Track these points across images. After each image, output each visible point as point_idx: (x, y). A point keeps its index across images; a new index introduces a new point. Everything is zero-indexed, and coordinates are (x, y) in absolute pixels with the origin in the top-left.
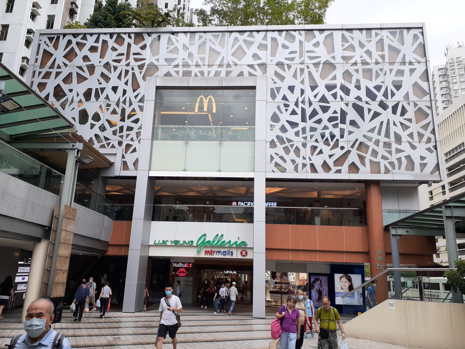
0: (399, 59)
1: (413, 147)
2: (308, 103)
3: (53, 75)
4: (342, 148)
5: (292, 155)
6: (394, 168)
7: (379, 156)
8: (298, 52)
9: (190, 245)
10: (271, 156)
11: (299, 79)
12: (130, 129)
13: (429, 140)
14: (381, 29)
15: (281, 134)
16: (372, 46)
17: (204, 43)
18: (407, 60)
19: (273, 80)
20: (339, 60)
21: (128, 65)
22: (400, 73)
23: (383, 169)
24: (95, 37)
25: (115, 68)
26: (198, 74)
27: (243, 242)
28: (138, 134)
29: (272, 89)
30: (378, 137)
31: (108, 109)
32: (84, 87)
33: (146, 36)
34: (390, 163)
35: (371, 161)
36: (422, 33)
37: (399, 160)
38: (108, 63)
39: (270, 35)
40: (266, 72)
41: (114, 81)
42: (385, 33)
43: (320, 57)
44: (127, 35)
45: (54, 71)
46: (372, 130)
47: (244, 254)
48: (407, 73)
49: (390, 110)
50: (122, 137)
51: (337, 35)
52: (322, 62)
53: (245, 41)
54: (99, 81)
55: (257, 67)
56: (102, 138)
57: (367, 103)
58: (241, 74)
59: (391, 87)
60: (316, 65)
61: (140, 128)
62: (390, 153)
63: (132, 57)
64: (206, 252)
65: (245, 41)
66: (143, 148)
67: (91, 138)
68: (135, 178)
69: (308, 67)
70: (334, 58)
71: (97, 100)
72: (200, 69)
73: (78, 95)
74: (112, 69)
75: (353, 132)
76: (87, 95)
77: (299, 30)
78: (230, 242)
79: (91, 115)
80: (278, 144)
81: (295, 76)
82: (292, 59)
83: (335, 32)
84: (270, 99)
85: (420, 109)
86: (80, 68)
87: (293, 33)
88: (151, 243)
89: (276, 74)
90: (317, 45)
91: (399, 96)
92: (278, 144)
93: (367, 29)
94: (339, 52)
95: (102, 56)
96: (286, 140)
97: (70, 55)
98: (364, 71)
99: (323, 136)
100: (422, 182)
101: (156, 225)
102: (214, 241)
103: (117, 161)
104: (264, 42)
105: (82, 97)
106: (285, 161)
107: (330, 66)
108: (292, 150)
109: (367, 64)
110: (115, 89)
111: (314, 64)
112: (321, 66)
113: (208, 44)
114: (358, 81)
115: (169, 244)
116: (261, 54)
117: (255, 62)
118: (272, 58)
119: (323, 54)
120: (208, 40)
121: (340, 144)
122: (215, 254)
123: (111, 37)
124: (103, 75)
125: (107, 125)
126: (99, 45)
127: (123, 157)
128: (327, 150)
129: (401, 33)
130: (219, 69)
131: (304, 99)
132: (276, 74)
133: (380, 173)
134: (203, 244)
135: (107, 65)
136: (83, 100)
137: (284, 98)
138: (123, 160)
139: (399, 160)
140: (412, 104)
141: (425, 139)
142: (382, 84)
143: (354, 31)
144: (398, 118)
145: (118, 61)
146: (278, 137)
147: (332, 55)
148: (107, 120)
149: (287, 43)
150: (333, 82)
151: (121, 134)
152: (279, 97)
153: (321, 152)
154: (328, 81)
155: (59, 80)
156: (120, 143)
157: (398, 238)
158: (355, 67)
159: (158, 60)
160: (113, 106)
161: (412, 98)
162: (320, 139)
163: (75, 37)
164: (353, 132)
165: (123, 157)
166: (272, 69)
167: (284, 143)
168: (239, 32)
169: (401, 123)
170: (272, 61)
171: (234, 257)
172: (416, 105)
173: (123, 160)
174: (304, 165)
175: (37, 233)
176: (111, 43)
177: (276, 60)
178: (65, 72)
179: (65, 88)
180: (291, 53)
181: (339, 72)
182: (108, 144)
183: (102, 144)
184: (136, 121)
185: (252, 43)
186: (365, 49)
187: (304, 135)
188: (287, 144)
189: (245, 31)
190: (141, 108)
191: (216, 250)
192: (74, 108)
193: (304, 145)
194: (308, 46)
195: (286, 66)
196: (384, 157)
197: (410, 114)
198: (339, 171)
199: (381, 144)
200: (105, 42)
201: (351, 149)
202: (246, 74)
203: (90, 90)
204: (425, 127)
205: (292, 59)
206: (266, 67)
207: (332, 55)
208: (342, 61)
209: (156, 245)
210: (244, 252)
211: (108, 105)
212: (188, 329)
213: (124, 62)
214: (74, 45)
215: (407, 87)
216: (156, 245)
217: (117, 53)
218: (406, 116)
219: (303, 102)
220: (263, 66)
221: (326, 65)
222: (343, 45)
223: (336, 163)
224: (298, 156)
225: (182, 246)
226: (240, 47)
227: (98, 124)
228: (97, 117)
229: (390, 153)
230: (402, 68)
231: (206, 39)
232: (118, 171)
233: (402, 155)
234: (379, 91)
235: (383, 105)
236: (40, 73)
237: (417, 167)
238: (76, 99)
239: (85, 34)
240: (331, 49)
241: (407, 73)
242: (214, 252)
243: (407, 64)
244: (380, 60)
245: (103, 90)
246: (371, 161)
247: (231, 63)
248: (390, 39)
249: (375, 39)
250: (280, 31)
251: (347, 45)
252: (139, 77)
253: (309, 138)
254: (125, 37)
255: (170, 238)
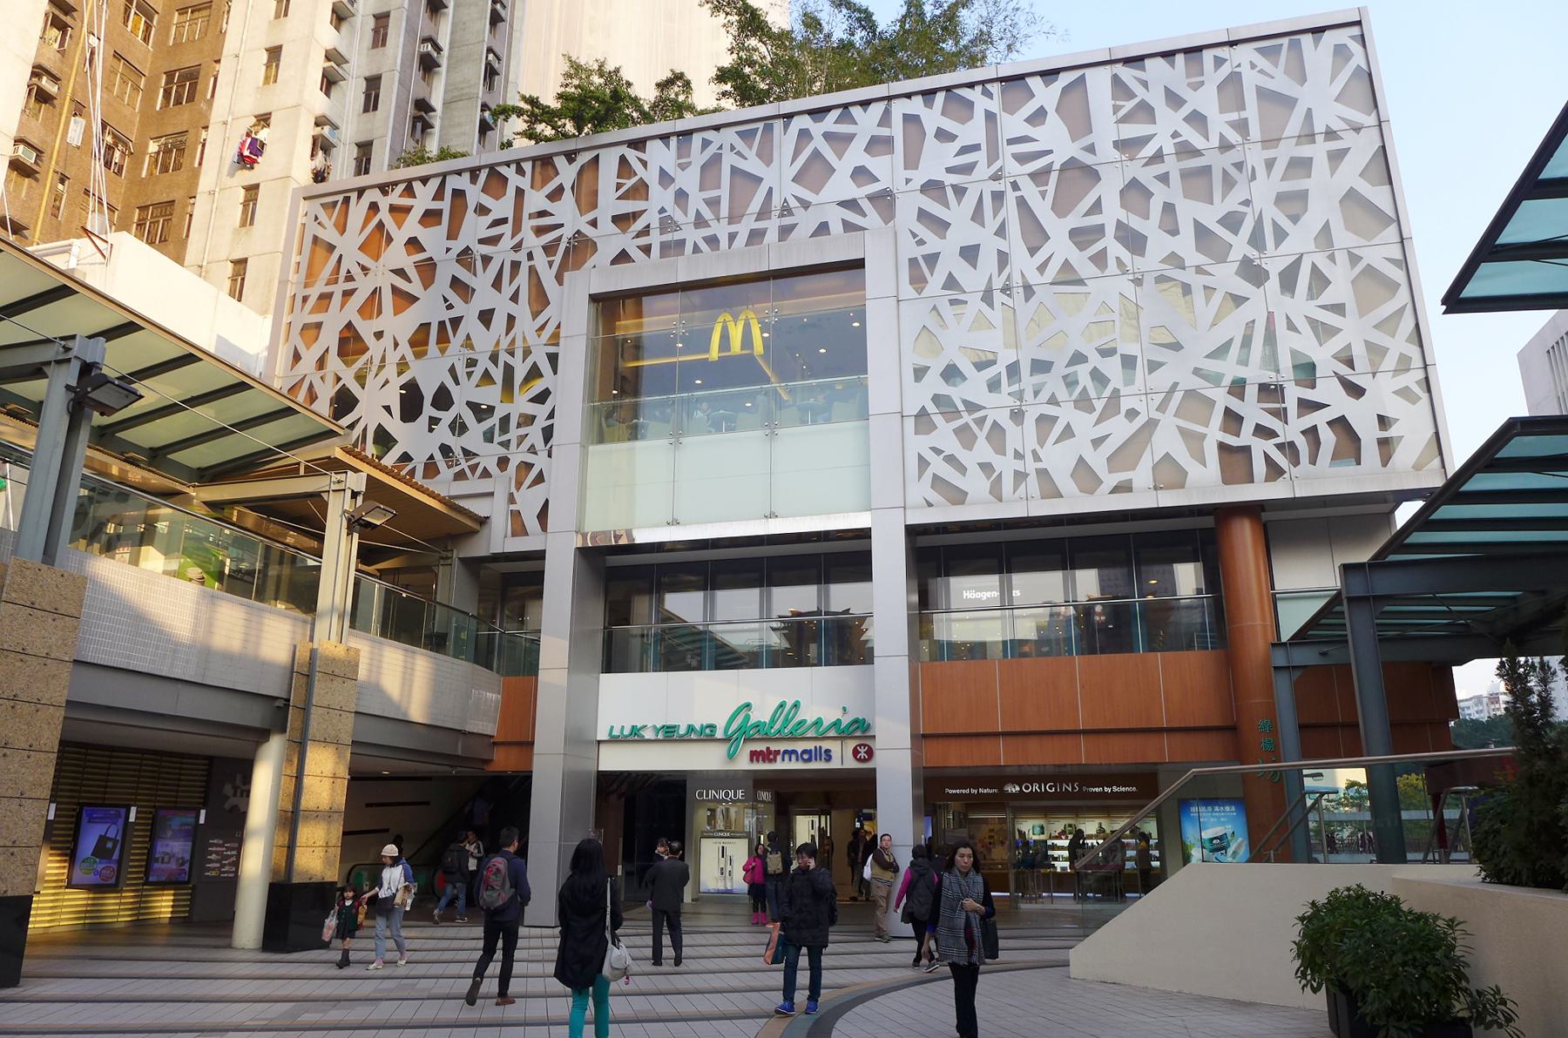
0: (1294, 126)
1: (1356, 391)
2: (1021, 290)
3: (337, 298)
4: (1132, 414)
5: (983, 450)
6: (1296, 461)
7: (1248, 428)
8: (984, 147)
9: (706, 735)
10: (921, 458)
11: (992, 224)
12: (528, 420)
13: (1403, 366)
14: (1232, 44)
15: (944, 389)
16: (1205, 100)
17: (716, 159)
18: (1319, 127)
19: (914, 235)
20: (1107, 152)
21: (517, 247)
22: (1301, 166)
23: (1259, 467)
24: (434, 184)
25: (487, 260)
26: (703, 246)
27: (856, 721)
28: (548, 433)
29: (913, 262)
30: (1242, 372)
31: (469, 374)
32: (411, 319)
33: (560, 162)
34: (1280, 447)
35: (1222, 447)
36: (1362, 40)
37: (1312, 433)
38: (468, 248)
39: (900, 108)
40: (892, 217)
41: (485, 297)
42: (1245, 54)
43: (1051, 152)
44: (513, 167)
45: (338, 290)
46: (1221, 352)
47: (862, 755)
48: (1321, 164)
49: (1273, 283)
50: (506, 444)
51: (1099, 82)
52: (1057, 166)
53: (828, 136)
54: (446, 300)
55: (866, 205)
56: (458, 452)
57: (1199, 270)
58: (823, 229)
59: (1272, 213)
60: (1039, 177)
61: (551, 416)
62: (1282, 415)
63: (528, 224)
64: (755, 756)
65: (828, 136)
66: (560, 466)
67: (431, 457)
68: (540, 555)
69: (1015, 186)
70: (1091, 149)
71: (443, 351)
72: (706, 232)
73: (396, 345)
74: (479, 264)
75: (1161, 365)
76: (419, 341)
77: (983, 83)
78: (818, 723)
79: (428, 394)
80: (938, 419)
81: (977, 216)
82: (967, 169)
83: (1088, 72)
84: (908, 291)
85: (1370, 271)
86: (400, 272)
87: (965, 93)
88: (602, 735)
89: (923, 215)
90: (1038, 117)
91: (1300, 239)
92: (938, 419)
93: (1187, 51)
94: (1106, 128)
95: (452, 234)
96: (961, 407)
97: (378, 239)
98: (1186, 175)
99: (1070, 382)
100: (616, 369)
101: (612, 684)
102: (773, 720)
103: (495, 511)
104: (884, 132)
105: (405, 350)
106: (962, 469)
107: (1080, 173)
108: (982, 435)
109: (1197, 153)
110: (486, 317)
111: (1034, 176)
112: (1054, 176)
113: (729, 160)
114: (1169, 208)
115: (648, 735)
116: (877, 165)
117: (860, 193)
118: (909, 174)
119: (1056, 140)
120: (727, 148)
121: (1126, 404)
122: (779, 758)
123: (474, 179)
124: (456, 283)
125: (469, 417)
126: (445, 205)
127: (512, 500)
128: (1084, 424)
129: (1295, 47)
130: (761, 225)
131: (1008, 278)
132: (923, 215)
133: (1252, 481)
134: (743, 732)
135: (465, 257)
136: (410, 357)
137: (951, 283)
138: (513, 507)
139: (1312, 433)
140: (1342, 257)
141: (1390, 362)
142: (1242, 209)
143: (1147, 61)
144: (1300, 306)
145: (493, 241)
146: (937, 399)
147: (1086, 141)
148: (469, 404)
149: (949, 125)
150: (1094, 220)
151: (505, 438)
152: (936, 281)
153: (1068, 432)
154: (1075, 220)
155: (351, 313)
156: (503, 462)
157: (1297, 674)
158: (1159, 169)
159: (594, 223)
160: (484, 363)
161: (1343, 238)
162: (1062, 393)
163: (385, 193)
164: (1161, 365)
165: (512, 500)
166: (909, 203)
167: (957, 414)
168: (811, 112)
169: (1313, 323)
170: (908, 181)
171: (835, 764)
172: (1354, 259)
173: (513, 507)
174: (1020, 476)
175: (252, 716)
176: (475, 195)
177: (920, 177)
178: (364, 287)
179: (366, 329)
180: (965, 150)
181: (1109, 189)
182: (473, 468)
183: (457, 469)
184: (542, 398)
185: (849, 138)
186: (1186, 110)
187: (1015, 387)
188: (967, 418)
189: (828, 109)
190: (553, 359)
191: (782, 747)
192: (387, 382)
193: (1017, 416)
194: (1013, 124)
195: (949, 191)
196: (1263, 432)
197: (1340, 291)
198: (1123, 488)
199: (1252, 392)
200: (459, 194)
201: (1156, 415)
202: (836, 227)
203: (425, 327)
204: (1388, 325)
205: (967, 169)
206: (892, 204)
207: (1086, 141)
208: (1116, 154)
209: (614, 740)
210: (862, 750)
211: (472, 363)
212: (454, 969)
213: (507, 242)
214: (384, 215)
215: (1322, 208)
216: (614, 740)
217: (489, 219)
218: (1329, 297)
219: (1006, 289)
220: (885, 201)
221: (1068, 174)
222: (1116, 109)
223: (1116, 460)
224: (1000, 450)
225: (682, 740)
226: (816, 154)
227: (447, 417)
228: (443, 399)
229: (1282, 415)
230: (1305, 151)
231: (720, 148)
232: (498, 540)
233: (1319, 419)
234: (1236, 232)
235: (1253, 273)
236: (305, 299)
237: (1370, 450)
238: (393, 358)
239: (409, 182)
240: (1080, 124)
241: (1321, 164)
242: (777, 752)
243: (1320, 138)
244: (1233, 137)
245: (456, 322)
246: (1222, 447)
247: (793, 203)
248: (1261, 71)
249: (1213, 77)
250: (929, 94)
251: (1129, 105)
252: (548, 277)
253: (1029, 396)
254: (509, 172)
255: (651, 718)
